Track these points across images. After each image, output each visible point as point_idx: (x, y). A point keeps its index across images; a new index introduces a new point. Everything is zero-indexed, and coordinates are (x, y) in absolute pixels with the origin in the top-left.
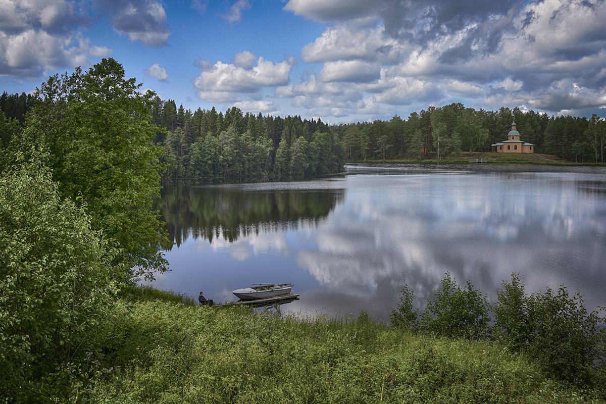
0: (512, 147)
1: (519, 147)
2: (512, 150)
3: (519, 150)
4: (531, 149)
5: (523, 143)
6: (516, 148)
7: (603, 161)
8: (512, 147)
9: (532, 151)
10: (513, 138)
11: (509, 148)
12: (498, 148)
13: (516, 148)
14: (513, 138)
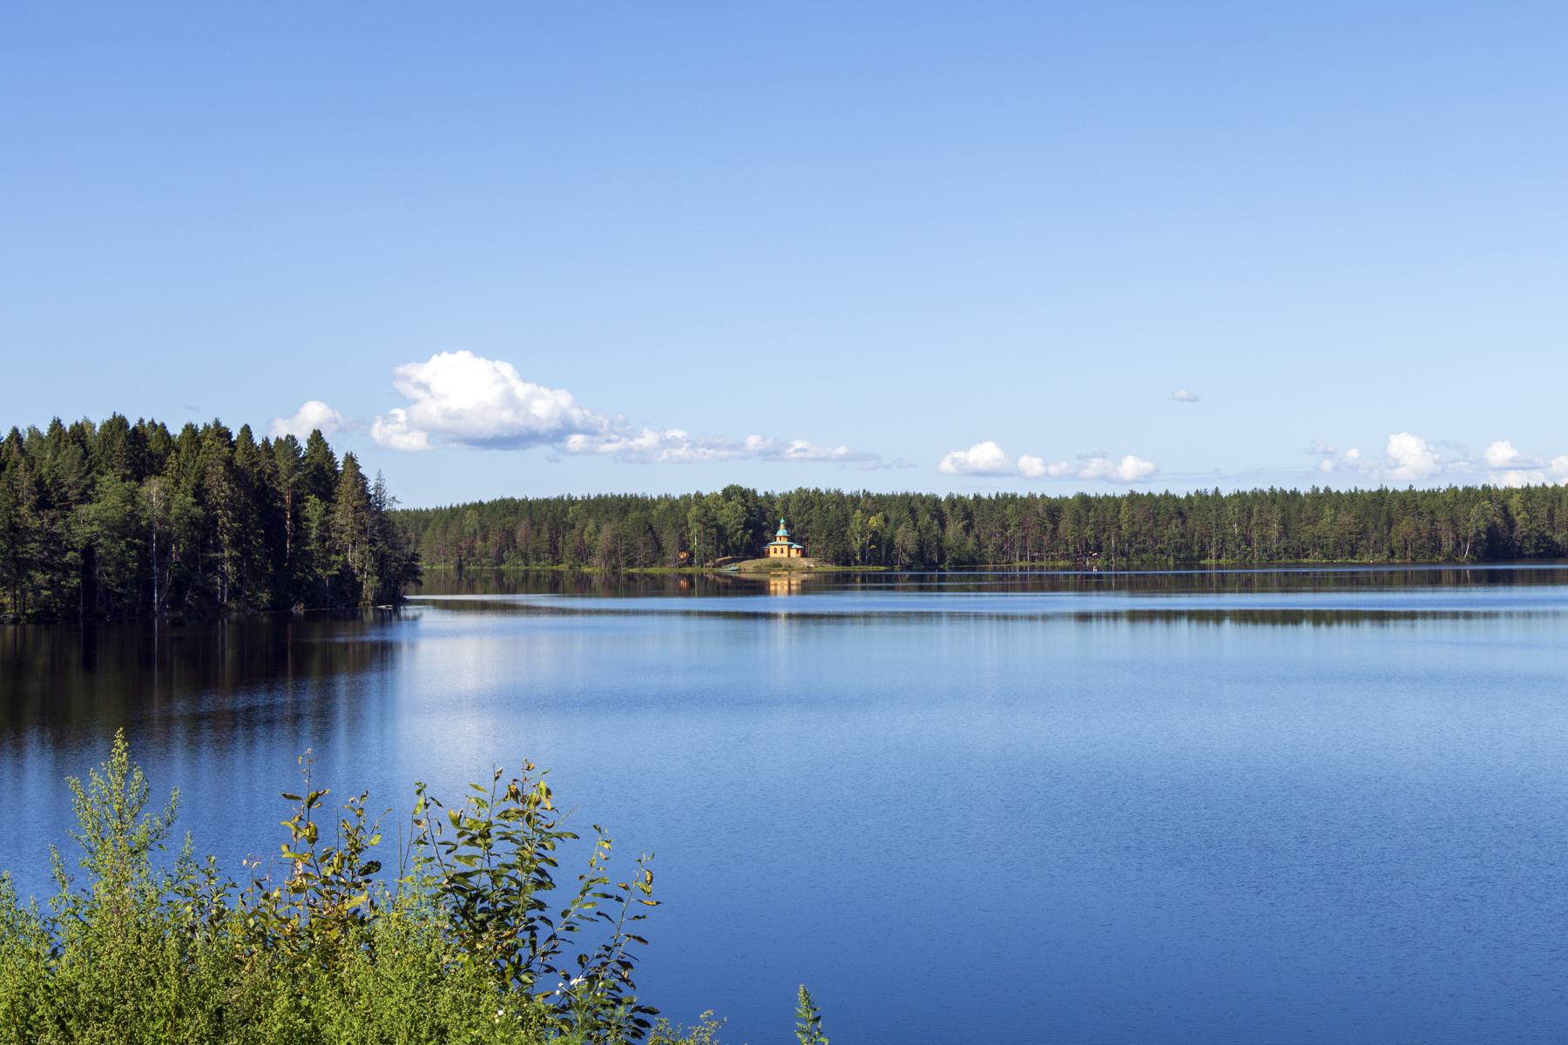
0: (779, 551)
4: (798, 552)
6: (782, 552)
8: (779, 551)
9: (799, 555)
11: (775, 552)
13: (782, 552)
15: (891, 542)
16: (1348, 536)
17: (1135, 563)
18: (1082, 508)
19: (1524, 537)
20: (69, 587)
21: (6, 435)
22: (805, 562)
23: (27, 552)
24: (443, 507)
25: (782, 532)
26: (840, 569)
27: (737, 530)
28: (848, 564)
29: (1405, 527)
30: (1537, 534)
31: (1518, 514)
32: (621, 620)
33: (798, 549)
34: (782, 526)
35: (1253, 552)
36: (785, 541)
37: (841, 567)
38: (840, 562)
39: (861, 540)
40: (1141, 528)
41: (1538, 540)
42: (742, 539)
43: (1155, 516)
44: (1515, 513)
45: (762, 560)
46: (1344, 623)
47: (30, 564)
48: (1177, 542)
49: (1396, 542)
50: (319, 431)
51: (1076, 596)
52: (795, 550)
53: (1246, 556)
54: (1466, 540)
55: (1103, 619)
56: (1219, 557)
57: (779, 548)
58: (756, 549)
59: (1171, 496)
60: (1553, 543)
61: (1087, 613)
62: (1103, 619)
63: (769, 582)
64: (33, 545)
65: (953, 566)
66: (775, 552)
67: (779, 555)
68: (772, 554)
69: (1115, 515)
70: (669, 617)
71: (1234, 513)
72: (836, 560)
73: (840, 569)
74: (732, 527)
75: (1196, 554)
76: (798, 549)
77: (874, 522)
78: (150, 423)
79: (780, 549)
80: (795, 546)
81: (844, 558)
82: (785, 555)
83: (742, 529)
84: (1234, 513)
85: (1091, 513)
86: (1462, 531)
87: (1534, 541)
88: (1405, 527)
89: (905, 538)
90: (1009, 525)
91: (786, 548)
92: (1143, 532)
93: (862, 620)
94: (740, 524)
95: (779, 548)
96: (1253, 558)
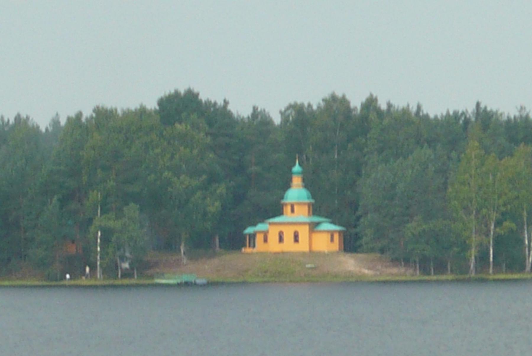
0: (288, 236)
1: (304, 232)
2: (289, 245)
3: (303, 246)
4: (332, 240)
5: (318, 224)
6: (296, 239)
7: (496, 263)
8: (288, 236)
9: (335, 246)
10: (293, 211)
12: (259, 238)
13: (296, 239)
14: (293, 211)
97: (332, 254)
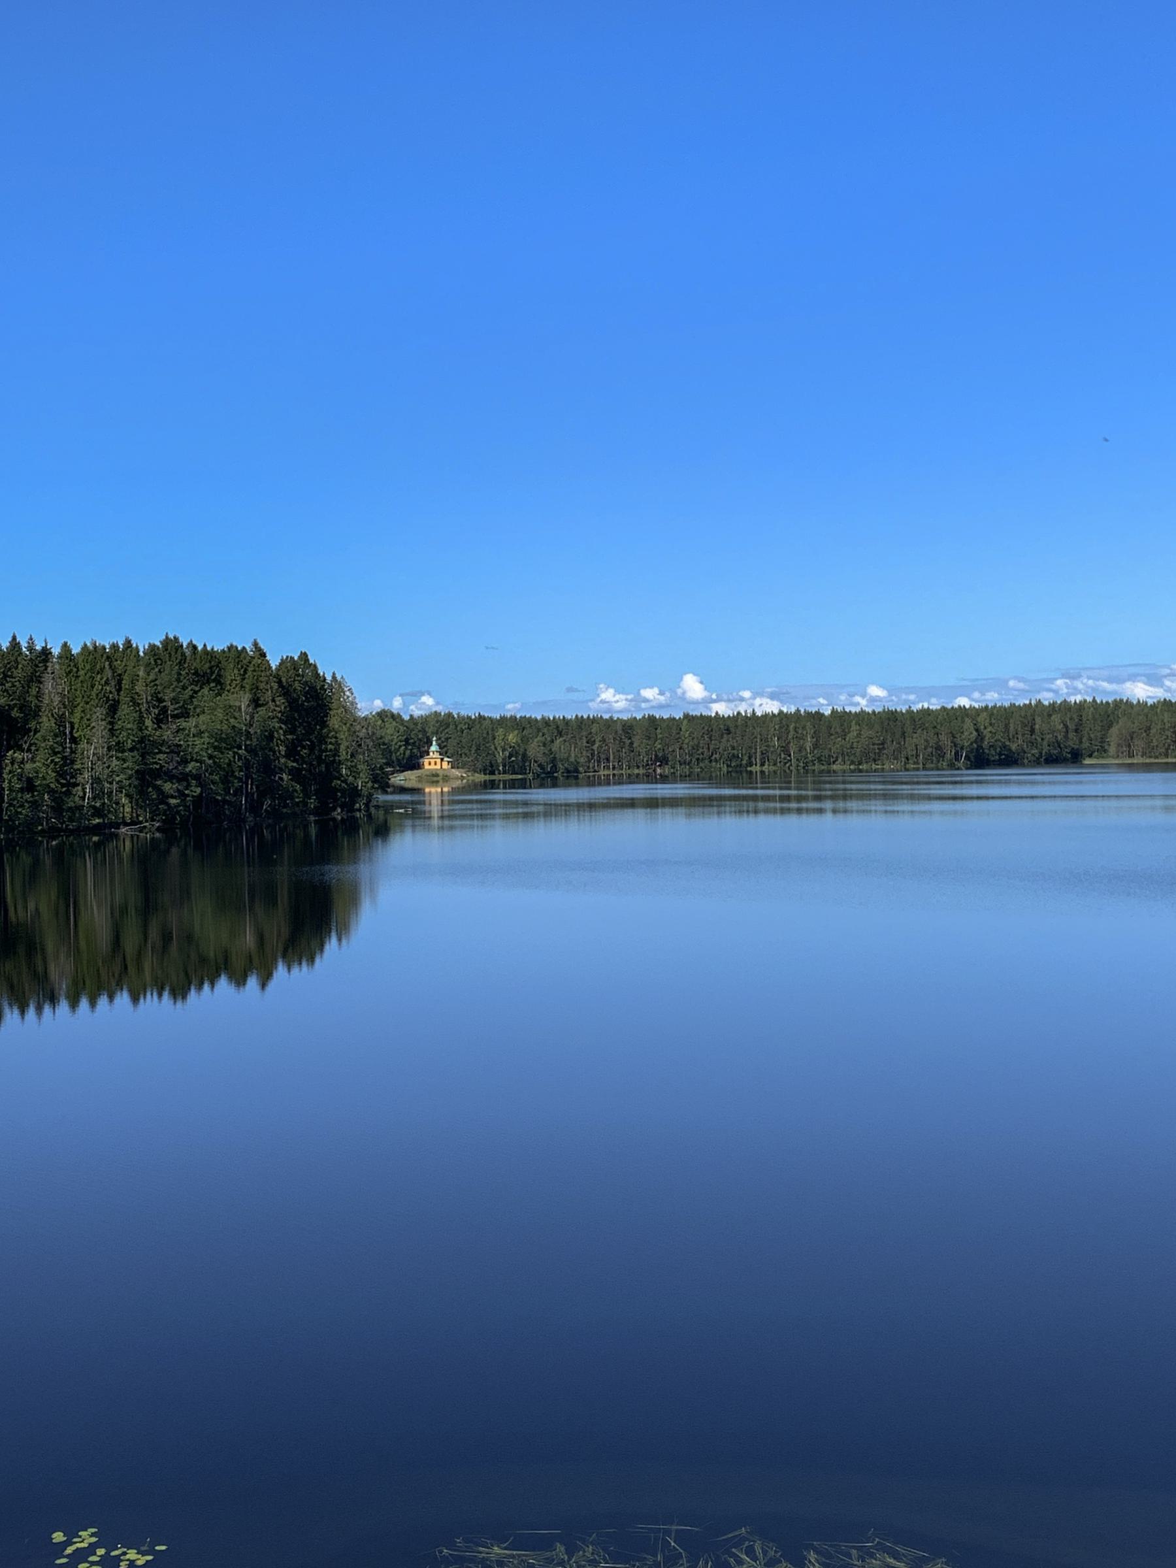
0: (433, 763)
4: (448, 764)
6: (436, 764)
8: (433, 763)
9: (450, 766)
11: (430, 764)
13: (436, 764)
15: (524, 755)
16: (872, 747)
17: (696, 770)
18: (651, 726)
19: (991, 746)
20: (193, 796)
21: (5, 645)
22: (456, 773)
23: (156, 763)
24: (585, 717)
25: (434, 748)
26: (487, 777)
27: (400, 746)
28: (492, 773)
29: (917, 739)
30: (1000, 744)
31: (985, 728)
32: (1075, 804)
33: (449, 762)
34: (434, 743)
35: (791, 760)
36: (437, 755)
37: (488, 776)
38: (488, 772)
39: (503, 754)
40: (699, 743)
41: (1001, 748)
42: (404, 754)
43: (709, 732)
44: (982, 727)
45: (420, 771)
46: (520, 820)
47: (158, 774)
48: (729, 753)
49: (910, 751)
50: (305, 653)
51: (571, 799)
52: (447, 763)
53: (786, 763)
54: (962, 748)
55: (745, 814)
56: (762, 765)
57: (433, 761)
58: (413, 764)
59: (463, 718)
60: (1010, 750)
61: (987, 796)
62: (745, 814)
63: (424, 790)
64: (161, 756)
65: (565, 774)
66: (430, 764)
67: (433, 767)
68: (427, 766)
69: (677, 732)
70: (964, 802)
71: (775, 729)
72: (484, 771)
73: (487, 777)
74: (396, 744)
75: (744, 762)
76: (449, 762)
77: (512, 738)
78: (189, 644)
79: (433, 761)
80: (446, 759)
81: (490, 769)
82: (438, 767)
83: (404, 745)
84: (775, 729)
85: (659, 731)
86: (958, 741)
87: (998, 749)
88: (917, 739)
89: (535, 750)
90: (594, 741)
91: (439, 761)
92: (701, 745)
93: (1101, 798)
94: (403, 741)
95: (433, 761)
96: (791, 765)
97: (448, 769)
